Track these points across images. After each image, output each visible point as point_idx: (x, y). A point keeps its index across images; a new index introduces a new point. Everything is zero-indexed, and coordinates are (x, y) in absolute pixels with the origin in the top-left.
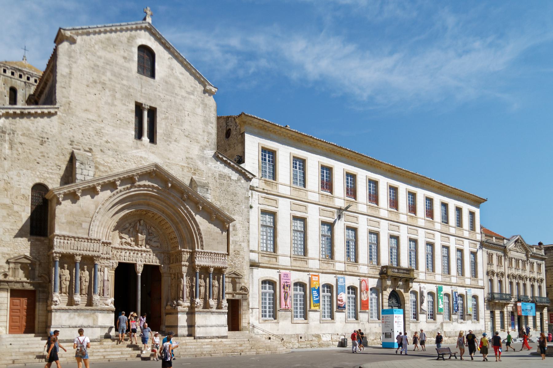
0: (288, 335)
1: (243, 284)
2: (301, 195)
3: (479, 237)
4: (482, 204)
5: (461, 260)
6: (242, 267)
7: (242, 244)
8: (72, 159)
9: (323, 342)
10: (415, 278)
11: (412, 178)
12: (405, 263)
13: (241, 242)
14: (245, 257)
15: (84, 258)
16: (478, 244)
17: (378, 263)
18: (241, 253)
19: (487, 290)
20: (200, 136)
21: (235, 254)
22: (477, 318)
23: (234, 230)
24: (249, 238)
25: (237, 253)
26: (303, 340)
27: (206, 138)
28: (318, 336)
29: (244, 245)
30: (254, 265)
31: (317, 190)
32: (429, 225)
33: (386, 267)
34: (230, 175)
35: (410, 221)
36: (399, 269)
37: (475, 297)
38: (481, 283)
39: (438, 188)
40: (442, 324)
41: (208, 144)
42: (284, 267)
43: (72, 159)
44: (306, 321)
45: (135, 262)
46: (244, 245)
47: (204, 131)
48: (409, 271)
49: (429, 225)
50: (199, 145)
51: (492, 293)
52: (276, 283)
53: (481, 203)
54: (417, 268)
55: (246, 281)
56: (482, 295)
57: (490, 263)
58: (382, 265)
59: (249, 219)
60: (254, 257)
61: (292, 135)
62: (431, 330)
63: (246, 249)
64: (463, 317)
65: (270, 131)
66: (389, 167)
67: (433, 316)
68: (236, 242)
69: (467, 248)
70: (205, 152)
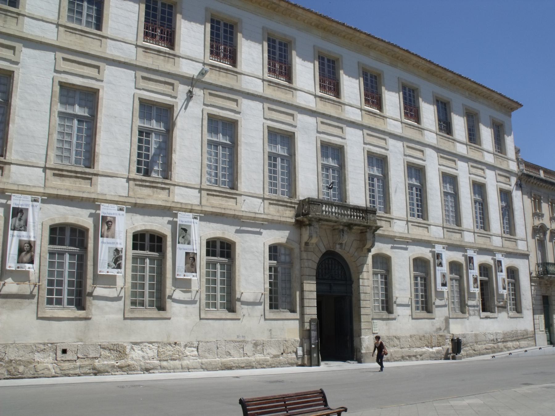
0: (26, 346)
3: (513, 166)
5: (482, 206)
8: (2, 175)
9: (130, 362)
11: (369, 46)
12: (357, 195)
16: (514, 180)
19: (534, 257)
22: (518, 309)
28: (119, 351)
31: (132, 38)
32: (410, 133)
33: (310, 202)
35: (368, 121)
36: (344, 206)
37: (513, 273)
38: (522, 247)
39: (428, 72)
40: (447, 320)
42: (21, 188)
43: (2, 175)
44: (81, 313)
45: (367, 342)
48: (365, 211)
49: (410, 133)
51: (544, 264)
53: (512, 109)
54: (387, 208)
56: (526, 270)
57: (537, 215)
58: (301, 198)
62: (421, 333)
64: (486, 306)
67: (425, 305)
69: (493, 184)
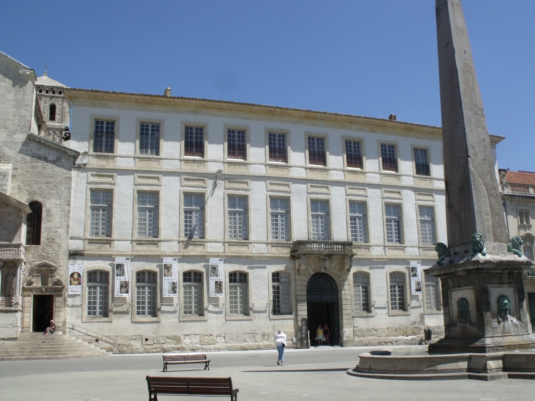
1: (57, 277)
2: (153, 166)
4: (500, 143)
6: (57, 256)
7: (59, 231)
10: (354, 255)
13: (57, 228)
14: (62, 245)
15: (274, 281)
17: (289, 238)
18: (57, 241)
20: (9, 122)
21: (49, 242)
23: (48, 216)
24: (68, 222)
25: (51, 240)
26: (149, 342)
27: (17, 122)
29: (62, 231)
30: (74, 255)
34: (47, 156)
41: (19, 128)
44: (155, 319)
46: (62, 231)
47: (15, 116)
48: (346, 244)
50: (8, 130)
52: (109, 272)
55: (62, 273)
59: (69, 201)
60: (76, 245)
61: (136, 99)
63: (64, 235)
65: (107, 100)
66: (303, 113)
67: (402, 305)
68: (49, 229)
70: (15, 136)
